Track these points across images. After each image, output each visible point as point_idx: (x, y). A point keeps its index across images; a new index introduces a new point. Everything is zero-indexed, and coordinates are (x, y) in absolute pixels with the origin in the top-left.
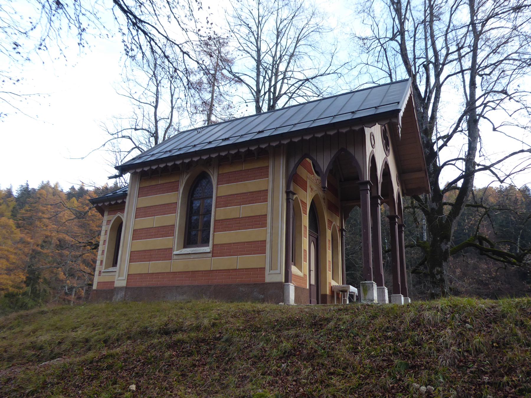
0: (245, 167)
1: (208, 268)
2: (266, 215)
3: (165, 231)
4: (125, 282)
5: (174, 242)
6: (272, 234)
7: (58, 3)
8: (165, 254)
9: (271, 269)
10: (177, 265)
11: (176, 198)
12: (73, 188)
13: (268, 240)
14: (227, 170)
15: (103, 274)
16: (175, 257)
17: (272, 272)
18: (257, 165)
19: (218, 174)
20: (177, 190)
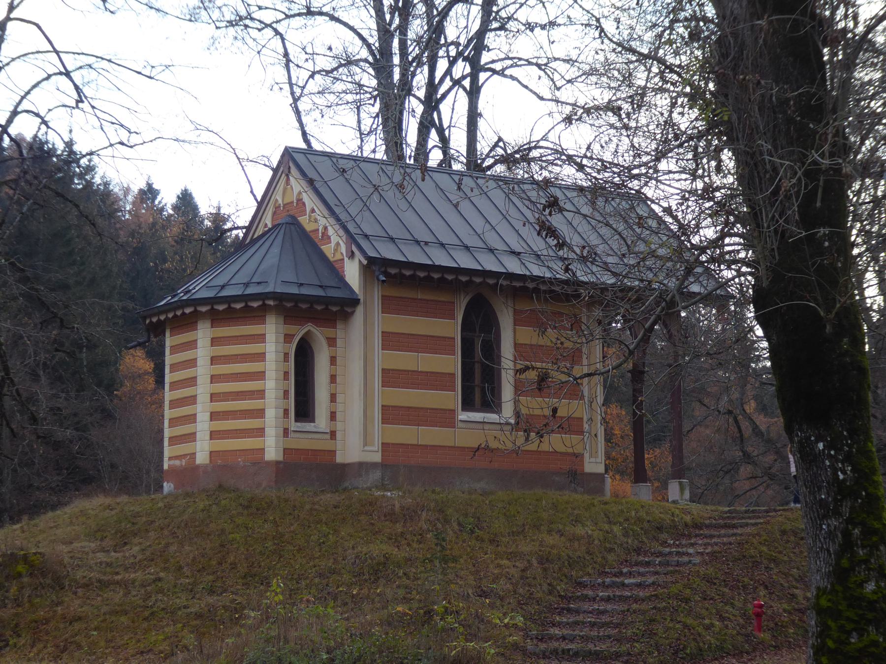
4: (380, 454)
5: (453, 398)
8: (445, 418)
9: (591, 456)
11: (452, 328)
14: (525, 306)
16: (460, 425)
17: (593, 460)
18: (443, 298)
20: (452, 317)
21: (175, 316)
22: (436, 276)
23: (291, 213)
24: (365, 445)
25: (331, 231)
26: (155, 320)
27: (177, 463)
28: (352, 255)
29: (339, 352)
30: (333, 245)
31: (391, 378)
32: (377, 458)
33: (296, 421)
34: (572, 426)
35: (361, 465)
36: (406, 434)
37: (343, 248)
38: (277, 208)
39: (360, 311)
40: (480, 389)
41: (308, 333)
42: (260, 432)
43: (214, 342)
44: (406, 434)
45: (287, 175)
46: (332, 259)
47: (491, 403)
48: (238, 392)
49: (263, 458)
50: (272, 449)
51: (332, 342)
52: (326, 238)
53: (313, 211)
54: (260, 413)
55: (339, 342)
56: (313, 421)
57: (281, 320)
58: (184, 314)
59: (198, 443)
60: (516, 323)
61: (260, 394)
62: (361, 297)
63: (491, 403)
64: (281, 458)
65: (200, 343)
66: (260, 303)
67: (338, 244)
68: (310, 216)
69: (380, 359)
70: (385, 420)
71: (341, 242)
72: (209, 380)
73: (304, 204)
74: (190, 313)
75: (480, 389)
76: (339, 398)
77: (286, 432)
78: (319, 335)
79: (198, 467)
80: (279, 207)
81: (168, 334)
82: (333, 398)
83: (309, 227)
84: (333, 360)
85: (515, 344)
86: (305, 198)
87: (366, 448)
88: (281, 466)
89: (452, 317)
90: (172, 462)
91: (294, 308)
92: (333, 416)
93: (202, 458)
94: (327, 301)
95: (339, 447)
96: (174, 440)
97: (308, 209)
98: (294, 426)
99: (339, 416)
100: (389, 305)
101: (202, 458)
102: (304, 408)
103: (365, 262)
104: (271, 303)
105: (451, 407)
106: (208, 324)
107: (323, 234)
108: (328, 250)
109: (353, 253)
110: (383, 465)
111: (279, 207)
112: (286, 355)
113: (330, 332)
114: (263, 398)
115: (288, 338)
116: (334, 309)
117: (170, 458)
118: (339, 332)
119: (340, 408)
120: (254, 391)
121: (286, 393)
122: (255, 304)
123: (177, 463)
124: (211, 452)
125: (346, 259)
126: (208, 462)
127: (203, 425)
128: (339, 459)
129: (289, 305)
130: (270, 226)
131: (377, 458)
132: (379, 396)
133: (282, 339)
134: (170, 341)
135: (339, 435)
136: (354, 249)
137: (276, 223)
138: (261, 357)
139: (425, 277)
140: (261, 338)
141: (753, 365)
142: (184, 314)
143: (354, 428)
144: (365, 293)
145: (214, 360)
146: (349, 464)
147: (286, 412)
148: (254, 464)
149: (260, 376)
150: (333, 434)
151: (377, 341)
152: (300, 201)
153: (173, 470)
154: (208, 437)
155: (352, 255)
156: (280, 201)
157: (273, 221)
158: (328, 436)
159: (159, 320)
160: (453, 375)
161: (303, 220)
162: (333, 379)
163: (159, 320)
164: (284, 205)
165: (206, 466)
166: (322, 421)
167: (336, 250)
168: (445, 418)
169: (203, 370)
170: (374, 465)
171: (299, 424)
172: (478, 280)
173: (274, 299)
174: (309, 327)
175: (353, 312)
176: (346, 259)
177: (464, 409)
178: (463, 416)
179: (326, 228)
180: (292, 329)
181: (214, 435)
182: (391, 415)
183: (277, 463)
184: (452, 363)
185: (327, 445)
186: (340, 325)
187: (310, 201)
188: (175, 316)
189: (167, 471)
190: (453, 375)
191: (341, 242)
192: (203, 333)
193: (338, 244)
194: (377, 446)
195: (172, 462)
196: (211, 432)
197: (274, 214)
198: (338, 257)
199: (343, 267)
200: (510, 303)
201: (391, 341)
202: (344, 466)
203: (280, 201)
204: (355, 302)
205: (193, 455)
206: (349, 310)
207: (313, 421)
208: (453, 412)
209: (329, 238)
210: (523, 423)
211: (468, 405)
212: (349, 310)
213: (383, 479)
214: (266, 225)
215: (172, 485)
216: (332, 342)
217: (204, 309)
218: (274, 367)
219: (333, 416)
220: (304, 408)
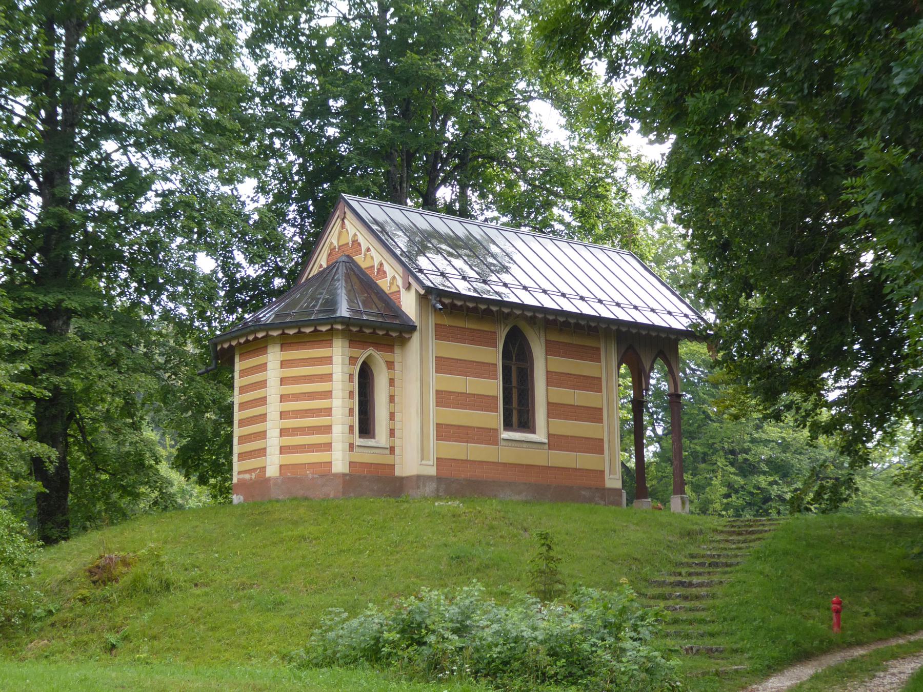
0: (576, 341)
1: (545, 464)
2: (601, 409)
3: (481, 402)
4: (435, 468)
5: (496, 419)
6: (609, 433)
7: (921, 316)
8: (488, 436)
9: (611, 473)
10: (504, 455)
11: (494, 355)
12: (207, 255)
13: (606, 439)
14: (554, 337)
15: (356, 449)
16: (503, 443)
17: (611, 476)
18: (486, 327)
19: (546, 341)
20: (495, 346)
21: (247, 341)
22: (483, 307)
23: (346, 253)
24: (422, 459)
25: (386, 268)
26: (226, 346)
27: (247, 476)
28: (408, 287)
29: (397, 375)
30: (389, 278)
31: (444, 398)
32: (432, 471)
33: (360, 437)
34: (595, 446)
35: (419, 477)
36: (457, 450)
37: (400, 282)
38: (332, 249)
39: (416, 337)
40: (519, 413)
41: (369, 356)
42: (328, 447)
43: (284, 364)
44: (457, 450)
45: (343, 220)
46: (387, 292)
47: (527, 424)
48: (306, 410)
49: (330, 470)
50: (339, 463)
51: (390, 365)
52: (381, 272)
53: (368, 250)
54: (328, 429)
55: (397, 366)
56: (373, 437)
57: (347, 344)
58: (256, 339)
59: (268, 457)
60: (548, 352)
61: (328, 411)
62: (417, 324)
63: (527, 424)
64: (347, 471)
65: (269, 366)
66: (328, 327)
67: (394, 278)
68: (365, 255)
69: (435, 381)
70: (439, 437)
71: (397, 276)
72: (279, 400)
73: (359, 244)
74: (263, 337)
75: (519, 413)
76: (397, 417)
77: (351, 446)
78: (379, 359)
79: (269, 479)
80: (335, 248)
81: (237, 359)
82: (392, 416)
83: (364, 265)
84: (392, 382)
85: (547, 372)
86: (361, 239)
87: (424, 462)
88: (348, 478)
89: (495, 346)
90: (241, 476)
91: (358, 333)
92: (392, 433)
93: (272, 471)
94: (388, 328)
95: (397, 461)
96: (243, 456)
97: (363, 249)
98: (359, 441)
99: (397, 433)
100: (442, 333)
101: (272, 471)
102: (366, 427)
103: (422, 292)
104: (339, 327)
105: (494, 426)
106: (278, 348)
107: (379, 270)
108: (384, 284)
109: (410, 284)
110: (439, 479)
111: (335, 248)
112: (351, 376)
113: (388, 356)
114: (331, 415)
115: (353, 360)
116: (394, 334)
117: (239, 473)
118: (397, 355)
119: (397, 426)
120: (321, 409)
121: (351, 411)
122: (324, 329)
123: (247, 476)
124: (281, 466)
125: (403, 291)
126: (278, 474)
127: (273, 441)
128: (398, 473)
129: (355, 329)
130: (325, 266)
131: (432, 471)
132: (434, 414)
133: (347, 361)
134: (238, 365)
135: (397, 451)
136: (411, 280)
137: (331, 263)
138: (328, 377)
139: (473, 308)
140: (328, 360)
141: (865, 364)
142: (256, 339)
143: (413, 441)
144: (421, 322)
145: (283, 381)
146: (407, 477)
147: (351, 428)
148: (322, 476)
149: (328, 394)
150: (392, 450)
151: (432, 365)
152: (356, 243)
153: (242, 483)
154: (278, 452)
155: (408, 287)
156: (335, 243)
157: (328, 260)
158: (388, 452)
159: (231, 346)
160: (495, 398)
161: (359, 259)
162: (392, 399)
163: (231, 346)
164: (340, 247)
165: (277, 478)
166: (381, 437)
167: (391, 284)
168: (488, 436)
169: (273, 390)
170: (429, 478)
171: (362, 440)
172: (518, 312)
173: (342, 323)
174: (371, 351)
175: (410, 338)
176: (403, 291)
177: (505, 429)
178: (506, 435)
179: (381, 264)
180: (356, 352)
181: (283, 450)
182: (445, 432)
183: (344, 475)
184: (494, 387)
185: (386, 459)
186: (397, 350)
187: (365, 240)
188: (247, 341)
189: (236, 485)
190: (495, 398)
191: (397, 276)
192: (273, 357)
193: (394, 278)
194: (432, 461)
195: (241, 476)
196: (281, 447)
197: (329, 255)
198: (394, 289)
199: (399, 298)
200: (542, 334)
201: (444, 365)
202: (401, 479)
203: (335, 243)
204: (413, 328)
205: (263, 469)
206: (407, 336)
207: (373, 437)
208: (496, 431)
209: (385, 273)
210: (556, 442)
211: (508, 425)
212: (407, 336)
213: (438, 490)
214: (321, 266)
215: (242, 498)
216: (390, 365)
217: (275, 333)
218: (340, 387)
219: (392, 433)
220: (366, 427)
